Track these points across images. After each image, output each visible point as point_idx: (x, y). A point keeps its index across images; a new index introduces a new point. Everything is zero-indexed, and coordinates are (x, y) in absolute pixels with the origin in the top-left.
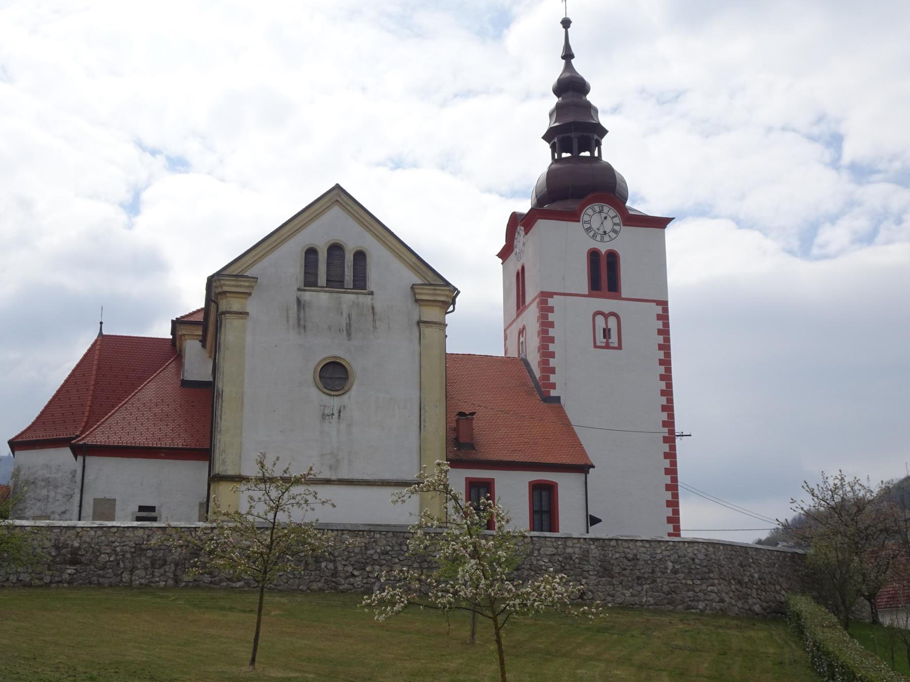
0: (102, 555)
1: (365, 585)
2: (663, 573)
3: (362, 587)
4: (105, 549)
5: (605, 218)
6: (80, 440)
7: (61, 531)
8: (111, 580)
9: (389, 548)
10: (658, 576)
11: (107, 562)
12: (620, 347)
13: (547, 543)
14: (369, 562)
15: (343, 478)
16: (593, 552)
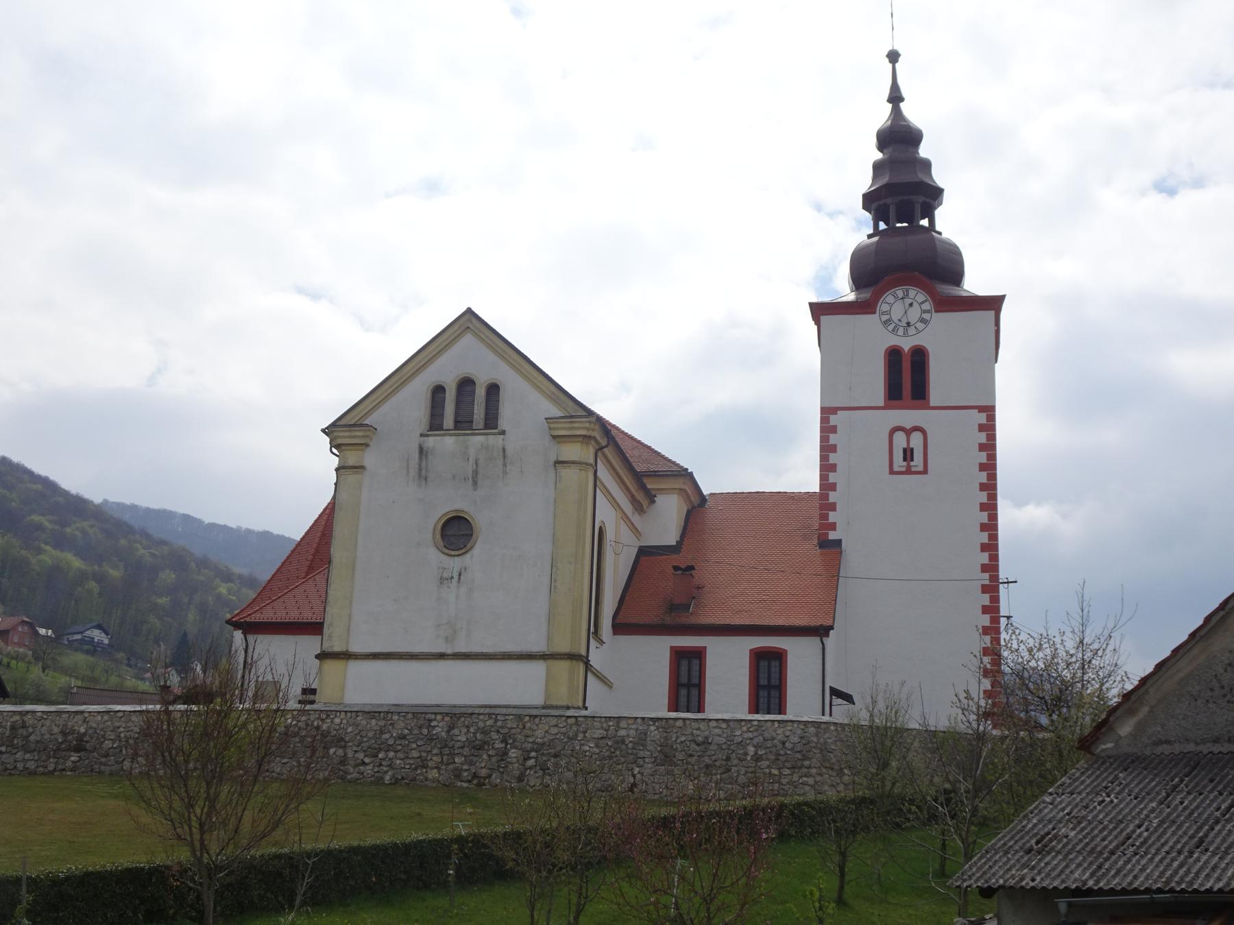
0: (106, 742)
1: (376, 775)
2: (740, 760)
3: (372, 776)
4: (110, 735)
5: (911, 305)
6: (241, 618)
7: (70, 716)
8: (112, 767)
9: (406, 731)
10: (734, 763)
11: (110, 749)
12: (925, 472)
13: (596, 724)
14: (383, 748)
15: (460, 651)
16: (652, 734)
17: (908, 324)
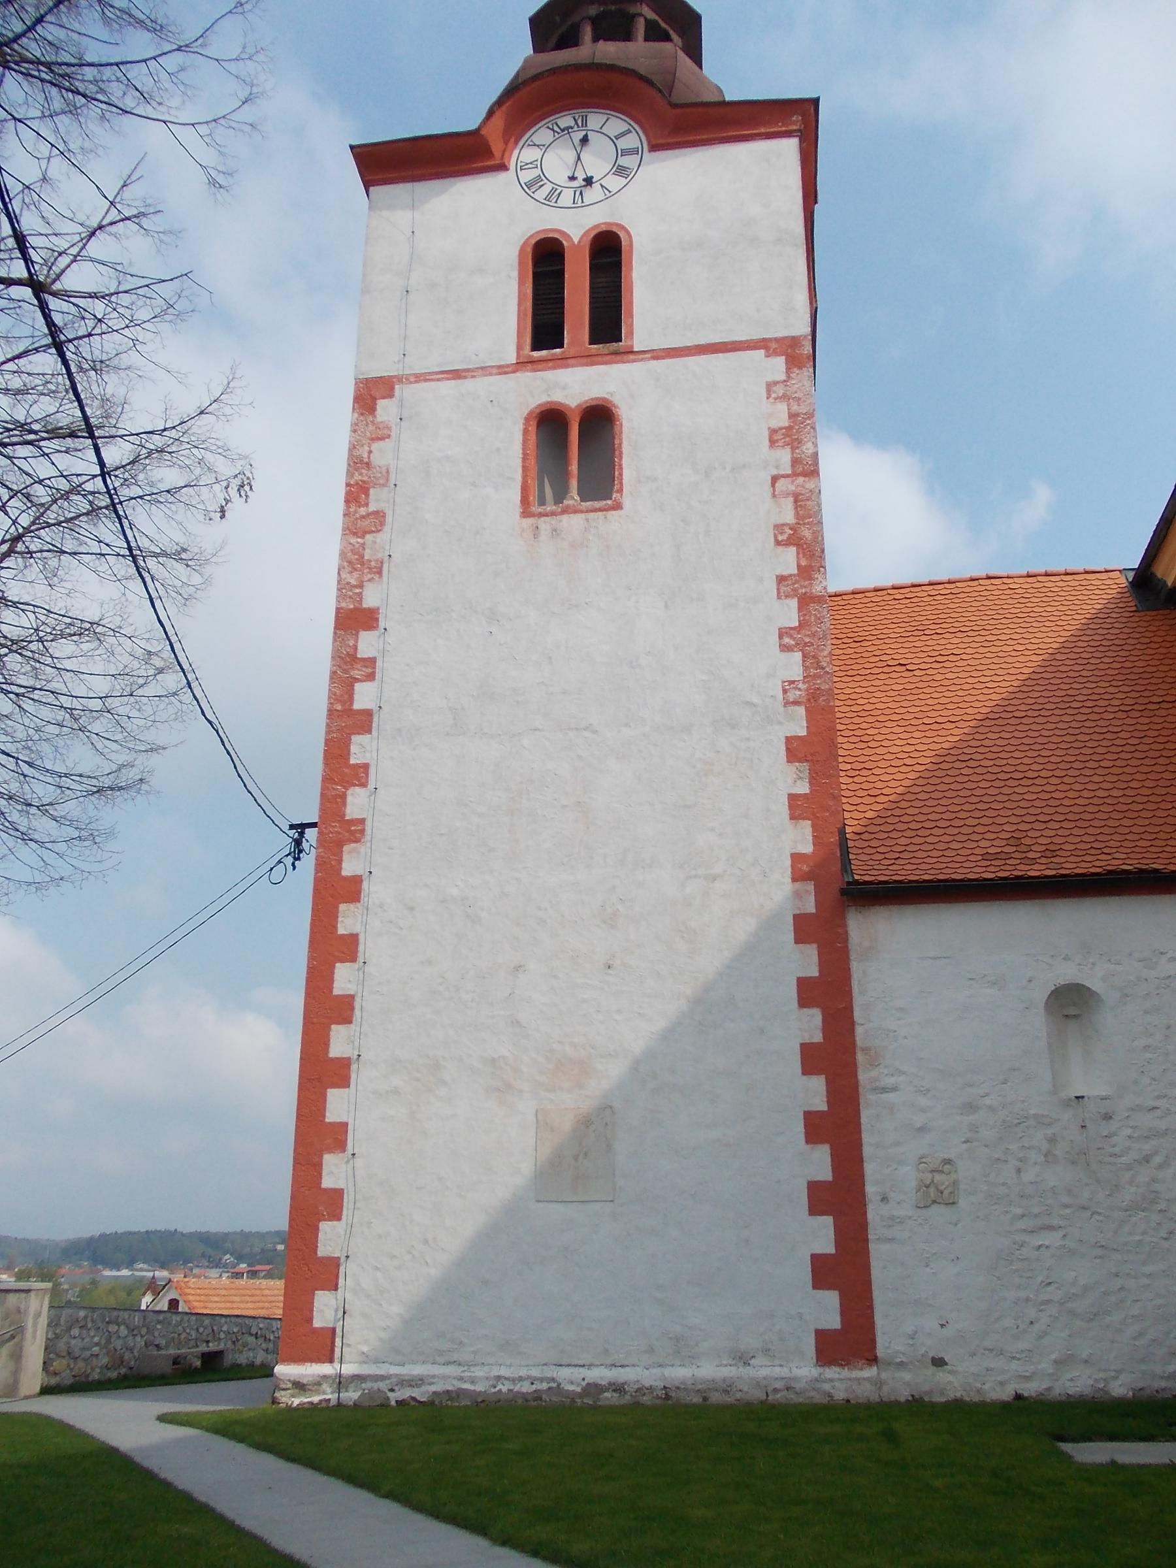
17: (589, 181)
